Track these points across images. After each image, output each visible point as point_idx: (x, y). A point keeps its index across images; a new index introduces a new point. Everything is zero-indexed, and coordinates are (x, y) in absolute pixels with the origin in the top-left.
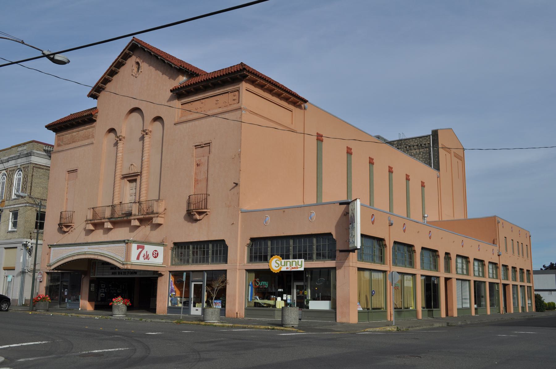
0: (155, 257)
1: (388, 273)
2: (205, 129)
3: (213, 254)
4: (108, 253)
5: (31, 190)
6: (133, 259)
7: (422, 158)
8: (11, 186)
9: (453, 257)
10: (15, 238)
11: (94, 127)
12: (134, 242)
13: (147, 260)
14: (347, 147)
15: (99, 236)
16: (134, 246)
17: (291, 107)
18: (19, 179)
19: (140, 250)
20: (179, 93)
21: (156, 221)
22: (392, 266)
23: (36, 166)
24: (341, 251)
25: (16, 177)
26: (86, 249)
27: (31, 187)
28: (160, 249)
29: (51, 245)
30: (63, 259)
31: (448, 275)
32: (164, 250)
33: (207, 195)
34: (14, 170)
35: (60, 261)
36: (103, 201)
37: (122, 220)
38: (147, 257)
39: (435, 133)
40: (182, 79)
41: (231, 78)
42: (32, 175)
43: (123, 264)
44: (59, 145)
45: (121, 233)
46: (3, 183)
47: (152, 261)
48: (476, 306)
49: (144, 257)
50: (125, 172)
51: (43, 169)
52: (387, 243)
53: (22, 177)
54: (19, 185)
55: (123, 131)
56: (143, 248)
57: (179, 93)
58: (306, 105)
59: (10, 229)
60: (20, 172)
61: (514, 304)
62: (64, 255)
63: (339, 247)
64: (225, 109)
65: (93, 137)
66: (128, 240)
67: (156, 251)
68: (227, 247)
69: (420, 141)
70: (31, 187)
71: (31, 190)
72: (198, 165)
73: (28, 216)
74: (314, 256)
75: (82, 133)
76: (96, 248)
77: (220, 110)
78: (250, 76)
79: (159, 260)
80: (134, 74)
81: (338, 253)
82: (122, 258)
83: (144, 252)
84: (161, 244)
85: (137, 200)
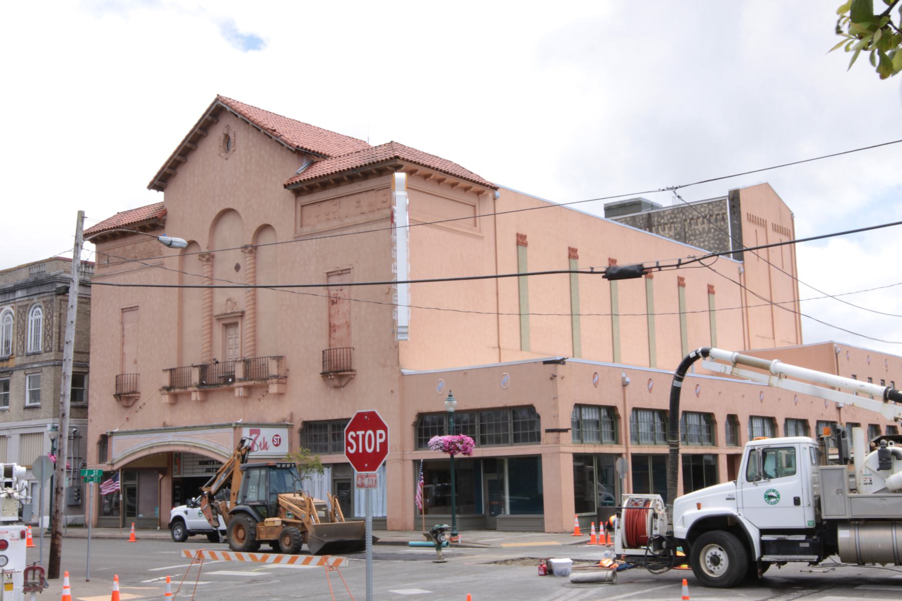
0: (277, 445)
1: (624, 456)
2: (340, 251)
4: (205, 443)
7: (713, 239)
8: (23, 332)
9: (743, 421)
10: (38, 418)
12: (245, 425)
13: (264, 451)
14: (570, 248)
15: (187, 414)
18: (38, 321)
22: (629, 446)
24: (548, 431)
25: (31, 318)
26: (169, 437)
28: (284, 433)
30: (133, 454)
31: (733, 451)
32: (290, 434)
34: (27, 306)
38: (265, 447)
39: (735, 197)
41: (376, 170)
42: (60, 314)
44: (100, 265)
46: (8, 327)
52: (621, 412)
54: (37, 330)
56: (258, 433)
58: (497, 193)
59: (28, 404)
61: (161, 571)
62: (136, 448)
63: (545, 424)
64: (371, 217)
69: (710, 210)
75: (141, 246)
76: (186, 436)
77: (362, 219)
78: (405, 164)
79: (283, 449)
81: (543, 434)
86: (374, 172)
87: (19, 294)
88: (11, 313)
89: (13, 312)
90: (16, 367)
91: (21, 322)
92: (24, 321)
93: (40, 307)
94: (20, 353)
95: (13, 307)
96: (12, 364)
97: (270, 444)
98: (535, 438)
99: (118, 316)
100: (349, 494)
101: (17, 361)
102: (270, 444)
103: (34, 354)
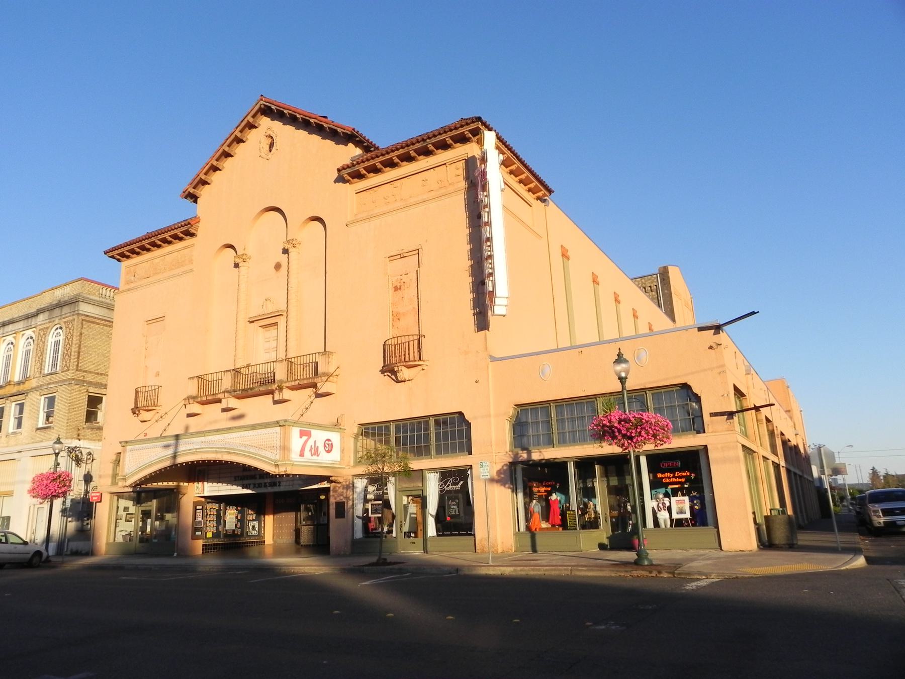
0: (328, 452)
3: (438, 438)
5: (78, 358)
6: (295, 456)
11: (193, 245)
12: (295, 423)
13: (315, 457)
16: (295, 431)
17: (530, 197)
18: (57, 343)
19: (305, 438)
20: (350, 174)
21: (323, 388)
23: (88, 319)
25: (51, 339)
27: (79, 353)
28: (335, 437)
29: (126, 442)
32: (342, 438)
33: (420, 338)
34: (47, 328)
35: (144, 468)
36: (217, 361)
37: (264, 386)
38: (315, 452)
40: (353, 151)
42: (81, 334)
43: (277, 466)
45: (258, 408)
47: (325, 458)
48: (654, 504)
49: (311, 450)
50: (254, 313)
51: (98, 324)
53: (61, 338)
54: (56, 351)
55: (248, 244)
56: (308, 434)
57: (350, 174)
59: (40, 425)
60: (59, 330)
65: (191, 262)
66: (286, 421)
67: (329, 440)
68: (469, 425)
70: (79, 353)
71: (78, 358)
72: (396, 289)
73: (70, 403)
74: (433, 452)
79: (335, 456)
80: (263, 155)
82: (275, 455)
83: (311, 443)
84: (336, 426)
85: (282, 355)
86: (450, 141)
87: (41, 317)
88: (32, 338)
89: (34, 336)
90: (32, 389)
91: (41, 344)
92: (44, 343)
93: (61, 328)
94: (37, 375)
95: (34, 332)
96: (28, 386)
97: (321, 449)
98: (701, 430)
99: (251, 103)
100: (465, 486)
101: (34, 383)
102: (321, 449)
103: (51, 374)
